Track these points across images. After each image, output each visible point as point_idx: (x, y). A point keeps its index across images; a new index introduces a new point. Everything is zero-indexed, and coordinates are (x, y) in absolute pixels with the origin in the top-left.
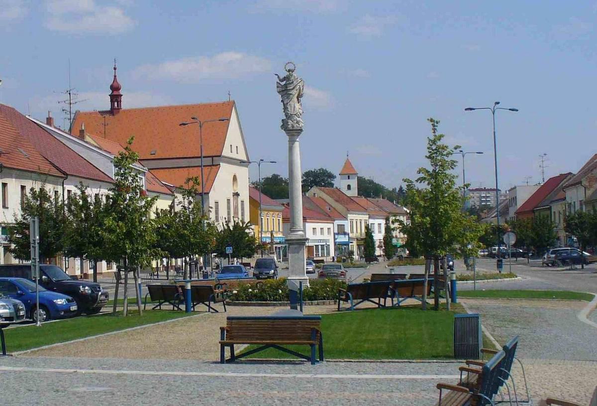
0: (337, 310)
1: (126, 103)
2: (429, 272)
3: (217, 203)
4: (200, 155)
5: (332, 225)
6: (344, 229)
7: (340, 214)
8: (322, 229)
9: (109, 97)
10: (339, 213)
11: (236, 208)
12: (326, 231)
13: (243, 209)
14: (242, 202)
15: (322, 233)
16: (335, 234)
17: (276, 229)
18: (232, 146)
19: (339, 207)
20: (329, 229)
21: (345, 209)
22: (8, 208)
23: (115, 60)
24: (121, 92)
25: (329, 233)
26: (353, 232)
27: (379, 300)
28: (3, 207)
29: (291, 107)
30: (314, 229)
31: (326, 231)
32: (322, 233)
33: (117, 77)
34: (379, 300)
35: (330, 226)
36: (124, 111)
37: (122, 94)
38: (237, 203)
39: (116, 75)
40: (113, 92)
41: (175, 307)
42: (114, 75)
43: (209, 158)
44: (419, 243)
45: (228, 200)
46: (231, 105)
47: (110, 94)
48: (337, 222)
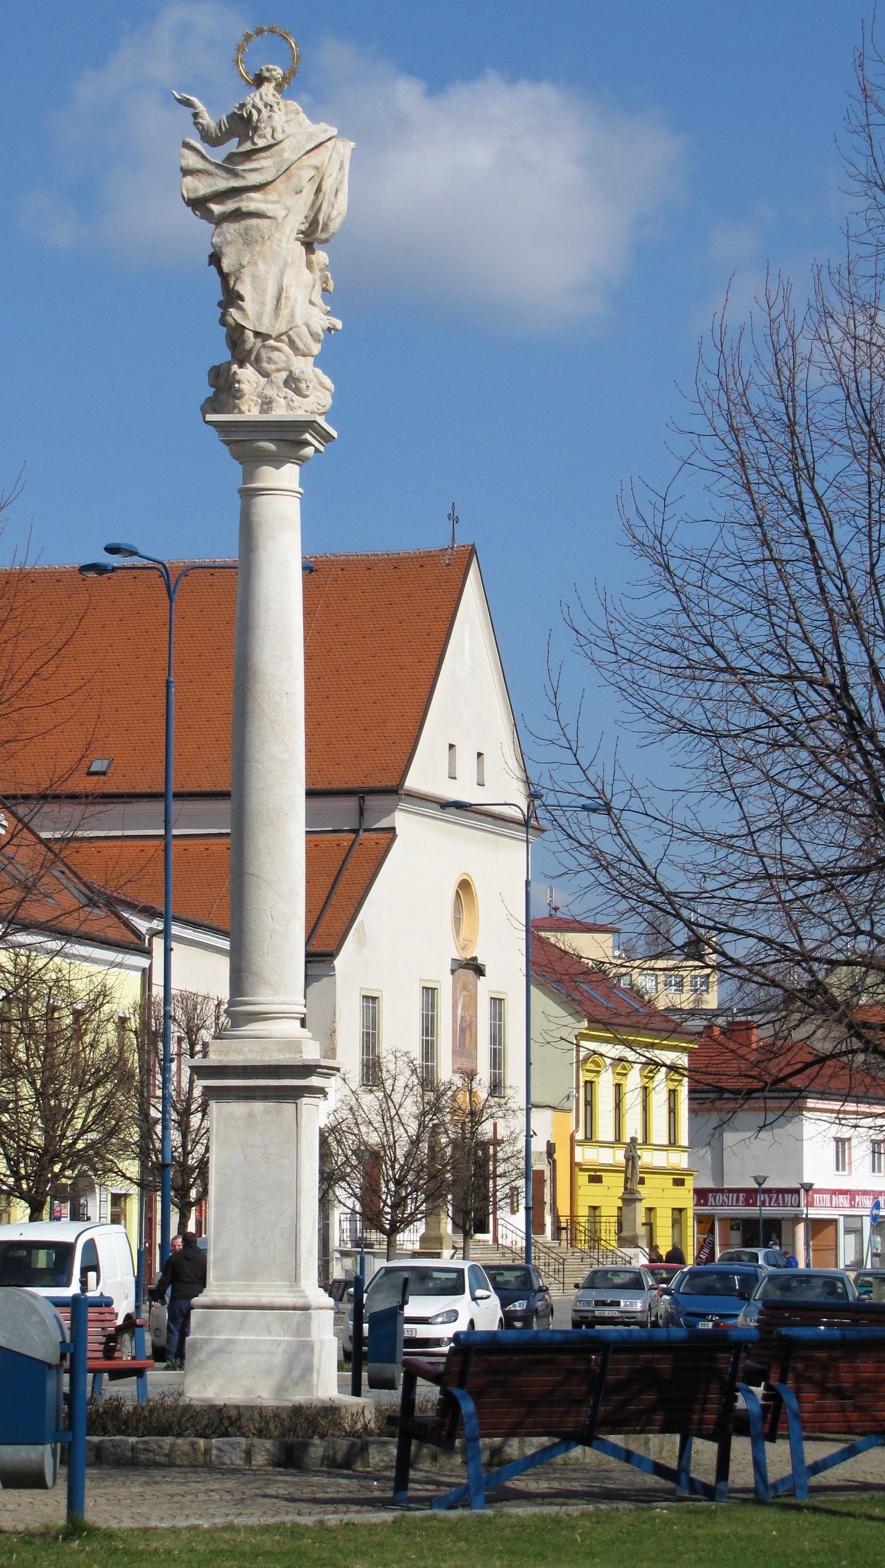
0: (100, 1354)
2: (147, 975)
3: (374, 999)
4: (161, 789)
13: (497, 1037)
14: (497, 1003)
17: (659, 1133)
18: (486, 757)
27: (685, 1447)
29: (259, 290)
34: (685, 1447)
43: (164, 787)
44: (876, 906)
45: (430, 993)
46: (472, 552)
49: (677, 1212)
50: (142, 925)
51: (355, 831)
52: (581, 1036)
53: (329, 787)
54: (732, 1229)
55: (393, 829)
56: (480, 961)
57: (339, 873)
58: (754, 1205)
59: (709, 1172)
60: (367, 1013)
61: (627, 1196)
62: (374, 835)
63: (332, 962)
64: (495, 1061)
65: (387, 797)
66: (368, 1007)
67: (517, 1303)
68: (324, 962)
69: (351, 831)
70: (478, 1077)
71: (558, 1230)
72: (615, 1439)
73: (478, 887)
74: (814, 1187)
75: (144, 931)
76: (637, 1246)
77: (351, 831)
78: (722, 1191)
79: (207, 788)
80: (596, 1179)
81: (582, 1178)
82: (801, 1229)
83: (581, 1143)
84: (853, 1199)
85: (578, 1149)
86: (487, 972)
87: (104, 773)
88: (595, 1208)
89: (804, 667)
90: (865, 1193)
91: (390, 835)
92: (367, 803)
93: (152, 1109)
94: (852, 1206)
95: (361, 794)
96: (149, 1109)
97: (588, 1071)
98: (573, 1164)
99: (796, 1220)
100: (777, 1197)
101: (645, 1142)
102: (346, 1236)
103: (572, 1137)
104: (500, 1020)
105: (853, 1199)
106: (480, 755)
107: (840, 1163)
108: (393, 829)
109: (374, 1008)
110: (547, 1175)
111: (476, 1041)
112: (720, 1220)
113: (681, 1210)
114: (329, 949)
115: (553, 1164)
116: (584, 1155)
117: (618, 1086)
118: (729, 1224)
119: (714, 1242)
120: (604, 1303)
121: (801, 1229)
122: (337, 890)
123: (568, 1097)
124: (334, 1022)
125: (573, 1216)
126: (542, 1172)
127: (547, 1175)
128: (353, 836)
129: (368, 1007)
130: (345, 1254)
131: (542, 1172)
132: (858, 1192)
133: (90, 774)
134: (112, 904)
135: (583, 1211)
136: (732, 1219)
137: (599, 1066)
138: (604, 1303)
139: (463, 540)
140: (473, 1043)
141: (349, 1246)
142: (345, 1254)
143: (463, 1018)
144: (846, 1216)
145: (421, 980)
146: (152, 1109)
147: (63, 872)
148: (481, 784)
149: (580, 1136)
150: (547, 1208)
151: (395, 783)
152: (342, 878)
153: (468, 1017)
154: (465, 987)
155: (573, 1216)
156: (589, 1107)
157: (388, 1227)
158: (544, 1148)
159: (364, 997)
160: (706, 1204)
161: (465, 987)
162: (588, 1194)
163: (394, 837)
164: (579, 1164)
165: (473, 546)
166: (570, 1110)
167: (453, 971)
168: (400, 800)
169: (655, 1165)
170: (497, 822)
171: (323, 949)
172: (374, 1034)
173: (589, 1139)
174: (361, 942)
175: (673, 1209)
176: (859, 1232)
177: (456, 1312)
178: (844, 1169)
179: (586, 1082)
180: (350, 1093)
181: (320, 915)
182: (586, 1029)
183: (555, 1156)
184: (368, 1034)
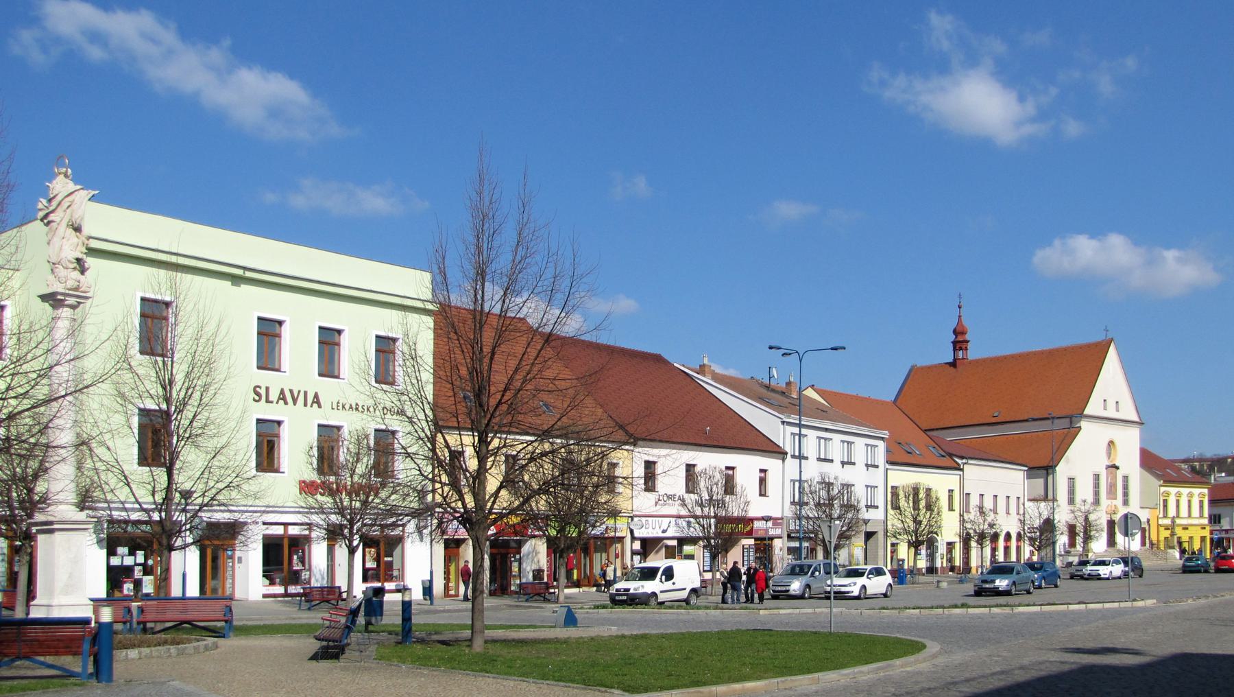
1: (974, 352)
3: (1073, 479)
9: (952, 345)
22: (954, 510)
23: (960, 295)
24: (967, 337)
28: (949, 509)
36: (971, 362)
39: (961, 314)
40: (956, 337)
41: (346, 593)
42: (958, 314)
46: (1112, 340)
47: (952, 340)
50: (959, 461)
52: (1161, 486)
55: (1080, 427)
71: (1152, 544)
72: (41, 658)
73: (1116, 442)
76: (1174, 548)
79: (1022, 419)
89: (31, 423)
93: (573, 535)
96: (573, 537)
98: (1159, 525)
102: (1062, 550)
106: (1105, 400)
110: (1147, 528)
113: (1205, 537)
115: (1149, 525)
120: (1078, 571)
125: (1158, 541)
127: (1147, 528)
130: (1061, 556)
134: (951, 455)
135: (1162, 539)
138: (1078, 571)
139: (1110, 336)
141: (1063, 553)
142: (1061, 556)
146: (573, 535)
149: (1161, 515)
155: (1158, 541)
158: (1146, 520)
161: (1111, 473)
167: (1106, 469)
173: (1165, 516)
174: (1068, 461)
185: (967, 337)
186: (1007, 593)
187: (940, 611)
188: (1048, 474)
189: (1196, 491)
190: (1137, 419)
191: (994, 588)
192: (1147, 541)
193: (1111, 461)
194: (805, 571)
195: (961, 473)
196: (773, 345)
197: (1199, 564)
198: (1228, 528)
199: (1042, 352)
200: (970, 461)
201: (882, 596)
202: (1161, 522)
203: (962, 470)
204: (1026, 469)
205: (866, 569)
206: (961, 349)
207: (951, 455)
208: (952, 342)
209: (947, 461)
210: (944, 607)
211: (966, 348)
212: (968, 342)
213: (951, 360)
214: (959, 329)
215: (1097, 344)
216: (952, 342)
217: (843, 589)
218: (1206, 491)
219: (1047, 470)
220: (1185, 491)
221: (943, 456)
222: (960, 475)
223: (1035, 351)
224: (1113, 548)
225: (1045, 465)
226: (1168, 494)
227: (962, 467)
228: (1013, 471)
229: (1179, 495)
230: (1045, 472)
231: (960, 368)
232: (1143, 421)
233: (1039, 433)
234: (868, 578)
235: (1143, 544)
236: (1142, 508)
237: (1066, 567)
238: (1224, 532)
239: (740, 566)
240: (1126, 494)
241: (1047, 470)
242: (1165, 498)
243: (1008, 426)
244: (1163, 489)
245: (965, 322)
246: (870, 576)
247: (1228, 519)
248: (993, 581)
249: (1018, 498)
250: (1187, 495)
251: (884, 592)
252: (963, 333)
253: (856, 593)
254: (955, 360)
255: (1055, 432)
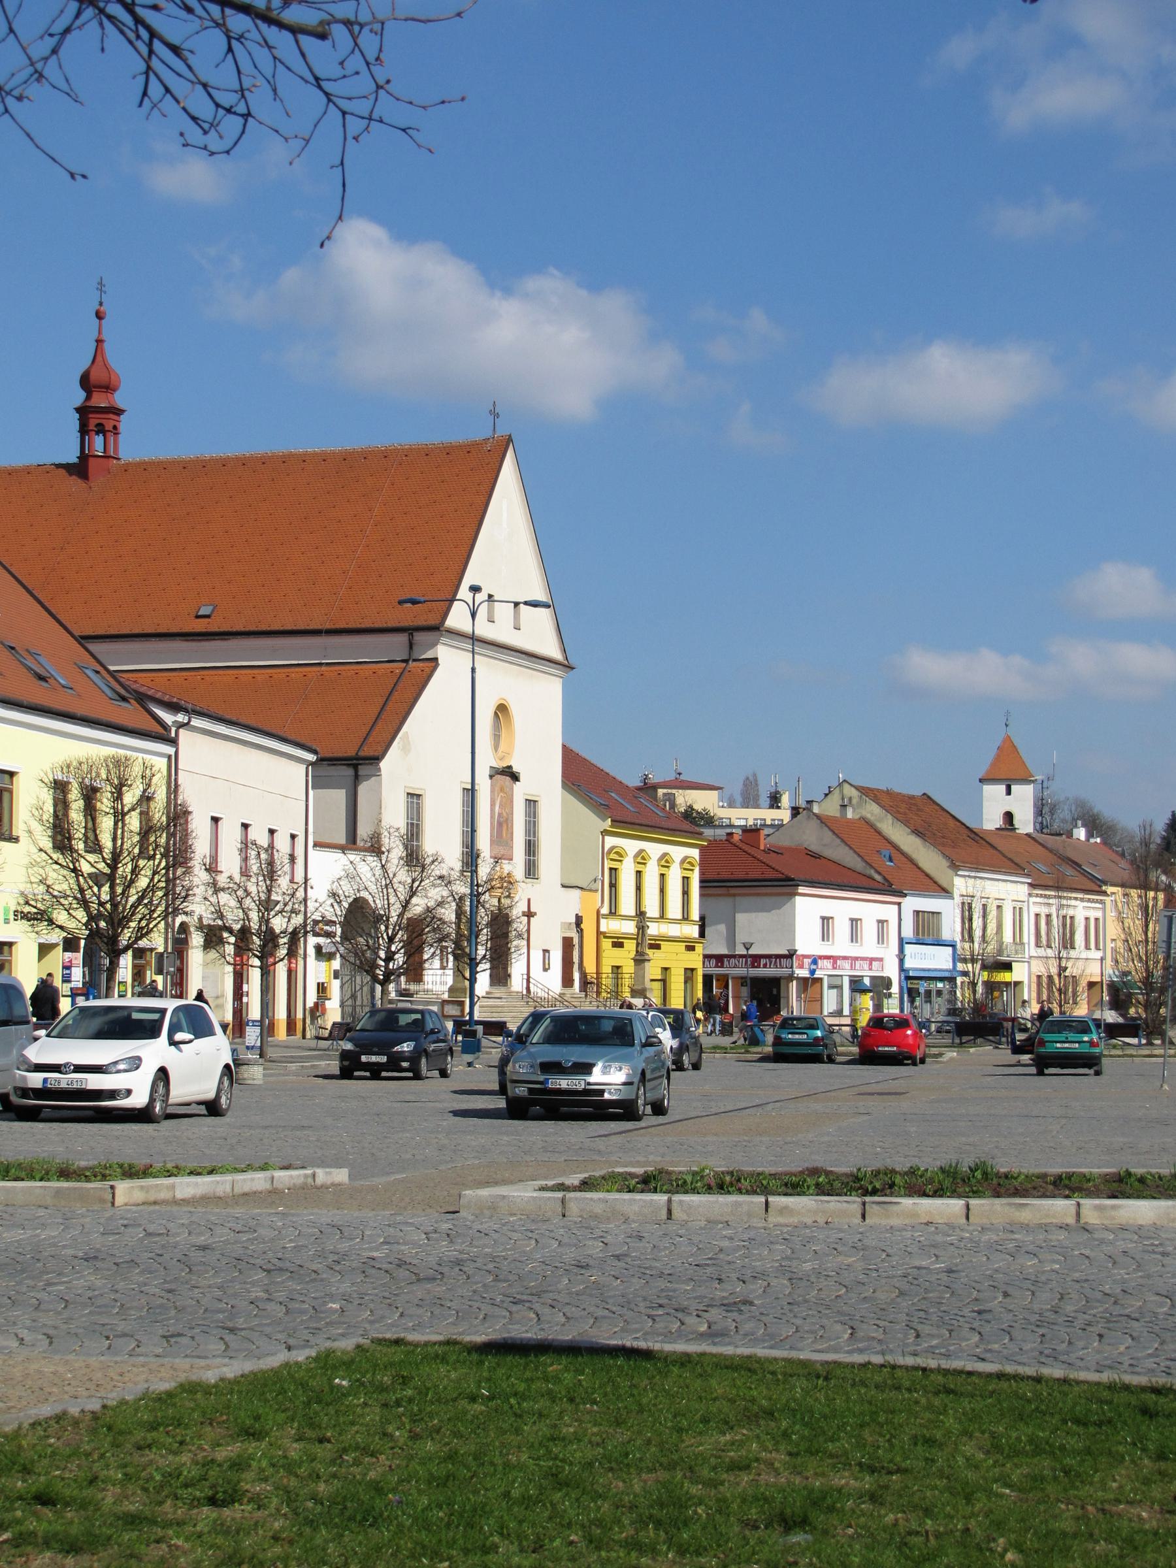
3: (419, 796)
5: (896, 907)
6: (939, 930)
7: (843, 841)
8: (854, 922)
9: (77, 416)
10: (847, 844)
11: (502, 826)
12: (869, 930)
14: (531, 804)
15: (854, 936)
16: (902, 942)
17: (674, 909)
19: (929, 858)
20: (881, 922)
21: (945, 863)
23: (101, 283)
25: (881, 938)
26: (971, 940)
30: (826, 920)
31: (869, 930)
32: (854, 936)
33: (106, 345)
35: (888, 912)
36: (126, 468)
37: (121, 406)
38: (509, 802)
39: (104, 336)
40: (88, 398)
42: (95, 335)
46: (509, 440)
48: (912, 903)
49: (689, 972)
50: (168, 718)
51: (406, 661)
52: (605, 833)
53: (385, 625)
54: (742, 985)
55: (435, 660)
56: (515, 769)
57: (390, 695)
58: (759, 966)
59: (724, 942)
60: (412, 808)
61: (638, 957)
62: (421, 664)
63: (378, 764)
64: (530, 850)
65: (430, 633)
66: (412, 802)
67: (405, 1045)
68: (371, 764)
69: (403, 661)
70: (482, 855)
71: (585, 984)
73: (514, 709)
74: (798, 953)
75: (170, 723)
77: (403, 661)
78: (734, 956)
79: (289, 627)
80: (618, 945)
81: (606, 944)
82: (794, 985)
83: (605, 916)
84: (835, 963)
85: (603, 922)
86: (522, 778)
87: (208, 616)
88: (618, 967)
90: (845, 958)
91: (433, 664)
92: (415, 638)
94: (834, 968)
95: (410, 631)
97: (612, 860)
98: (599, 933)
99: (791, 977)
100: (776, 962)
101: (662, 916)
103: (598, 912)
104: (535, 818)
105: (835, 963)
107: (825, 935)
108: (436, 659)
109: (418, 804)
111: (512, 833)
112: (733, 978)
113: (692, 970)
114: (376, 754)
115: (580, 931)
116: (607, 925)
117: (639, 873)
118: (740, 981)
119: (728, 995)
121: (794, 985)
122: (387, 708)
123: (595, 880)
124: (380, 813)
126: (572, 939)
127: (576, 941)
128: (404, 665)
129: (412, 802)
131: (572, 939)
132: (839, 958)
133: (198, 617)
134: (142, 699)
135: (606, 969)
136: (742, 978)
137: (622, 856)
139: (502, 431)
140: (509, 835)
143: (500, 815)
144: (829, 976)
145: (462, 782)
147: (97, 672)
148: (517, 628)
149: (605, 910)
150: (576, 967)
151: (438, 622)
152: (393, 698)
153: (505, 814)
154: (502, 790)
156: (613, 889)
157: (381, 977)
159: (408, 794)
160: (722, 966)
161: (502, 790)
162: (612, 957)
163: (437, 665)
164: (604, 933)
165: (510, 436)
166: (596, 891)
167: (491, 777)
168: (442, 635)
169: (670, 934)
170: (530, 659)
171: (371, 753)
172: (418, 825)
173: (613, 913)
174: (406, 749)
175: (686, 969)
176: (839, 987)
177: (139, 1059)
178: (828, 940)
179: (611, 869)
180: (348, 863)
181: (373, 726)
182: (611, 827)
183: (582, 926)
184: (412, 824)
185: (119, 399)
186: (625, 1111)
187: (1060, 1208)
188: (357, 779)
189: (678, 853)
190: (557, 655)
191: (586, 1092)
192: (576, 976)
193: (501, 759)
194: (419, 1016)
195: (170, 750)
196: (218, 138)
197: (817, 1039)
198: (725, 951)
199: (324, 458)
200: (197, 722)
201: (202, 1110)
202: (605, 926)
203: (173, 742)
204: (311, 757)
205: (163, 1012)
206: (101, 429)
207: (142, 699)
208: (78, 410)
209: (130, 713)
210: (761, 1185)
211: (115, 427)
212: (119, 412)
213: (72, 457)
214: (96, 376)
215: (470, 448)
216: (78, 410)
217: (94, 1082)
218: (695, 853)
219: (355, 767)
220: (655, 850)
221: (124, 699)
222: (169, 757)
223: (306, 454)
224: (503, 989)
225: (351, 753)
226: (620, 855)
227: (173, 735)
228: (284, 761)
229: (641, 858)
230: (350, 772)
231: (98, 480)
232: (572, 662)
233: (324, 668)
234: (173, 1043)
235: (567, 981)
236: (563, 886)
237: (331, 1037)
238: (713, 962)
239: (57, 982)
240: (531, 848)
241: (355, 767)
242: (614, 865)
243: (233, 643)
244: (610, 841)
245: (114, 357)
246: (179, 1036)
247: (722, 928)
248: (586, 1068)
249: (293, 837)
250: (636, 856)
251: (211, 1095)
252: (109, 388)
253: (139, 1100)
254: (84, 457)
255: (366, 670)
